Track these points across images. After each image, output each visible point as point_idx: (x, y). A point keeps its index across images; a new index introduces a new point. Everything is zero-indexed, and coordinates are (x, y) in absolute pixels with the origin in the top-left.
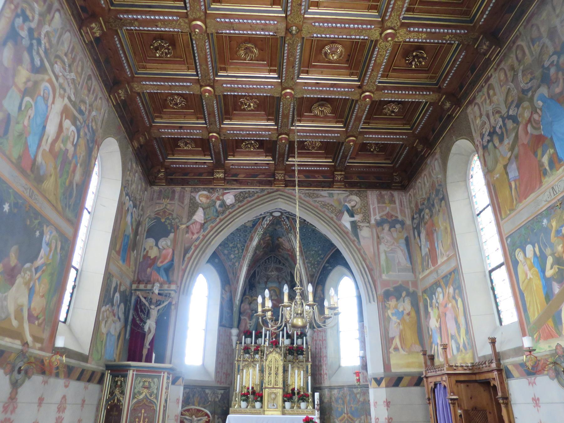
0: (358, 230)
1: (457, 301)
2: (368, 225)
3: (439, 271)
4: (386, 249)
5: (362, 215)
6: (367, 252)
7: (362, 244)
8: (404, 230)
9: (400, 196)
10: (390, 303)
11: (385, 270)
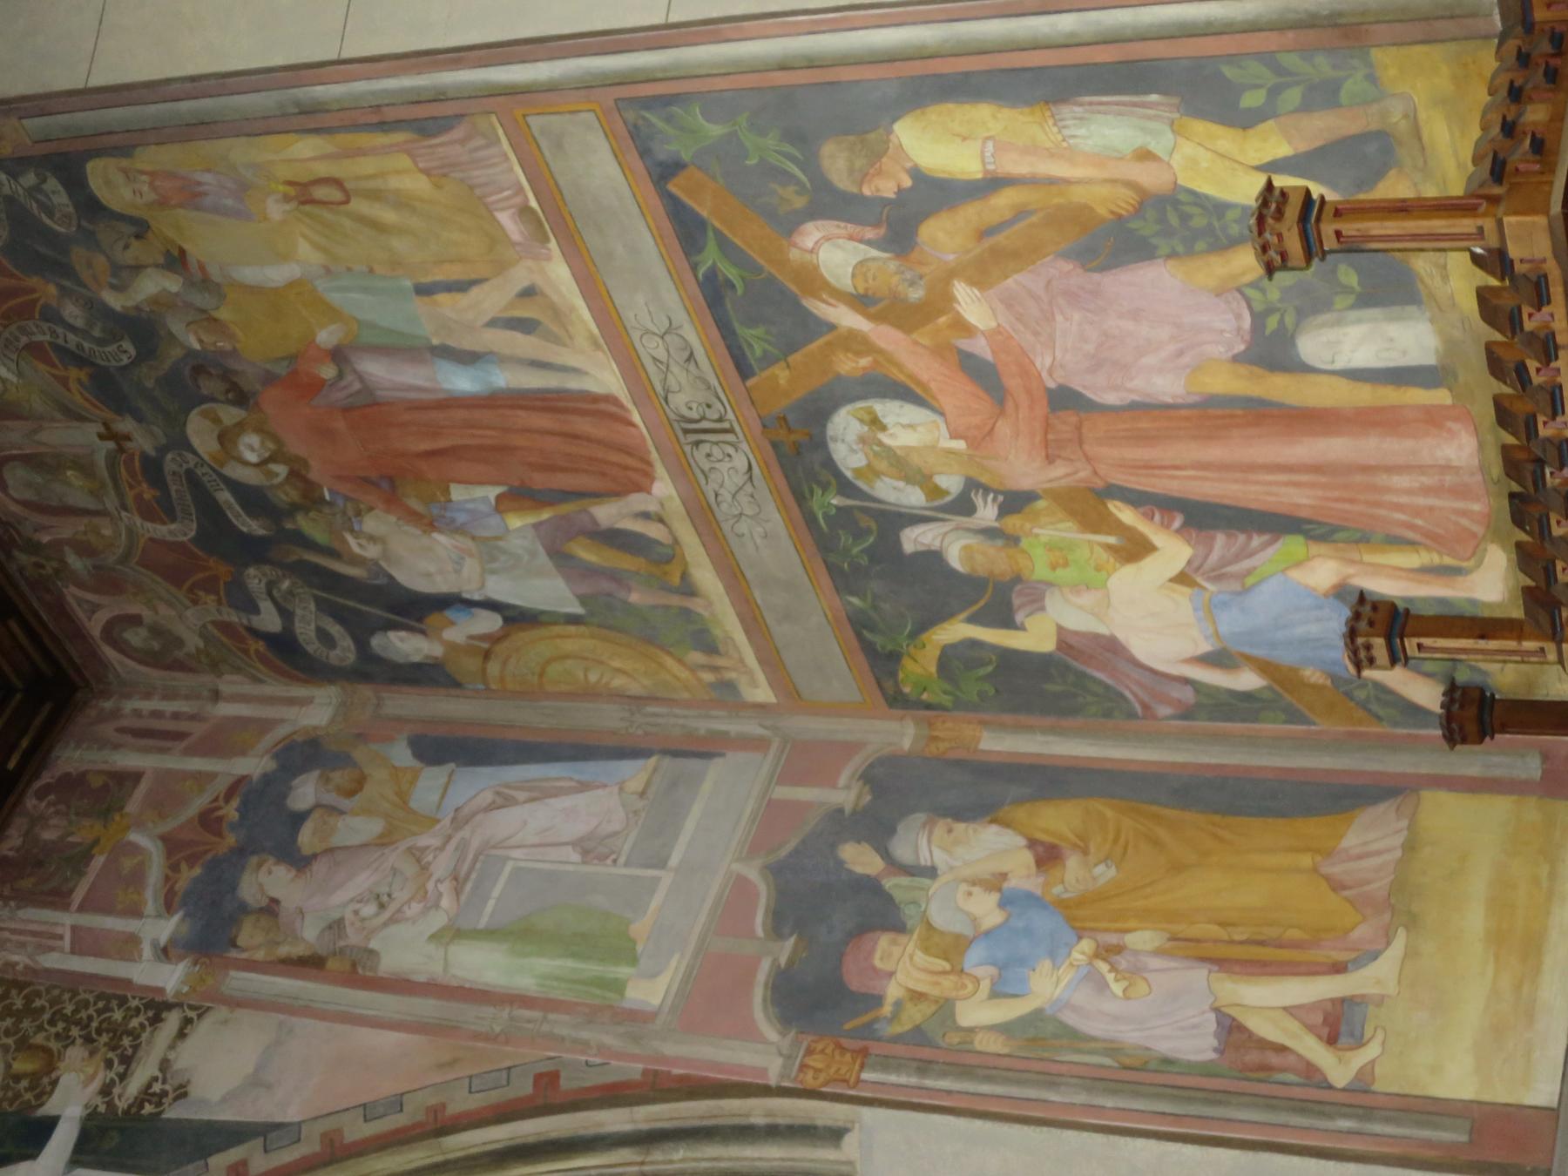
0: (173, 1112)
1: (936, 193)
2: (173, 1020)
3: (685, 400)
4: (438, 921)
5: (76, 1053)
6: (386, 1088)
7: (291, 1115)
8: (359, 754)
9: (108, 730)
10: (893, 992)
11: (593, 969)
